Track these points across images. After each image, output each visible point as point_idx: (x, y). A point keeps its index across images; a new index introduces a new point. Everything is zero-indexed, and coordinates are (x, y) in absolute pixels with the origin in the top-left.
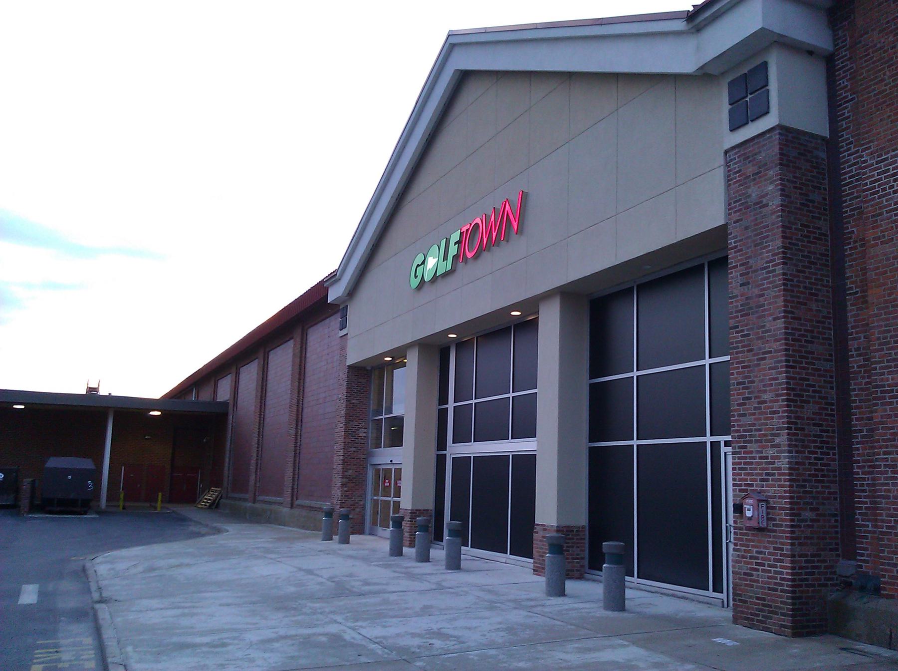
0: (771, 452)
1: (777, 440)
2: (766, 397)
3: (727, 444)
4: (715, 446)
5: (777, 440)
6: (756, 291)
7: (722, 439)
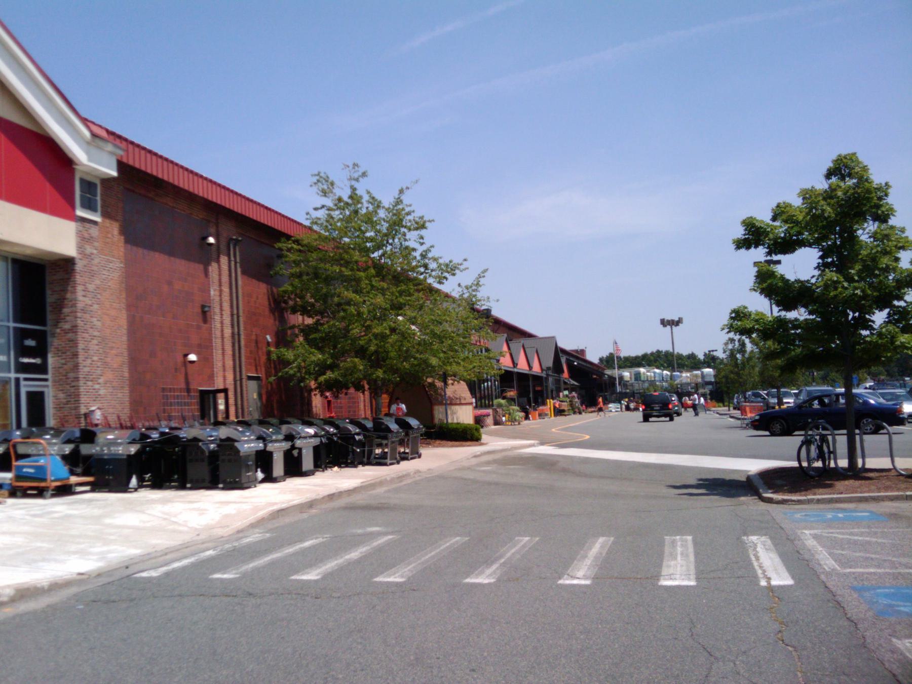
0: (97, 386)
2: (95, 358)
3: (26, 379)
4: (17, 380)
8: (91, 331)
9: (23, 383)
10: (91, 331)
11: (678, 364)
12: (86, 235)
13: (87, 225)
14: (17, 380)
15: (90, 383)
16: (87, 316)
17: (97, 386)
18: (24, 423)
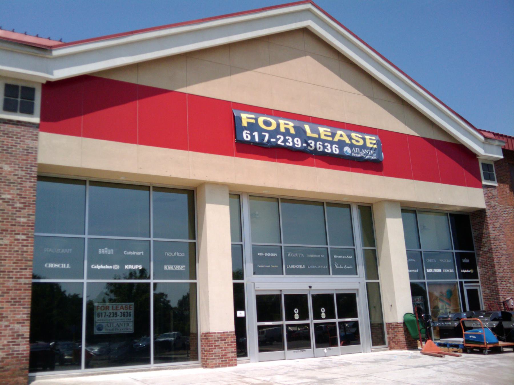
0: (509, 285)
1: (510, 281)
2: (505, 267)
4: (461, 283)
5: (510, 281)
6: (498, 234)
7: (463, 280)
8: (501, 251)
9: (464, 284)
10: (501, 251)
11: (256, 260)
12: (490, 195)
13: (490, 189)
14: (461, 283)
15: (504, 283)
16: (498, 242)
17: (509, 285)
18: (468, 309)
